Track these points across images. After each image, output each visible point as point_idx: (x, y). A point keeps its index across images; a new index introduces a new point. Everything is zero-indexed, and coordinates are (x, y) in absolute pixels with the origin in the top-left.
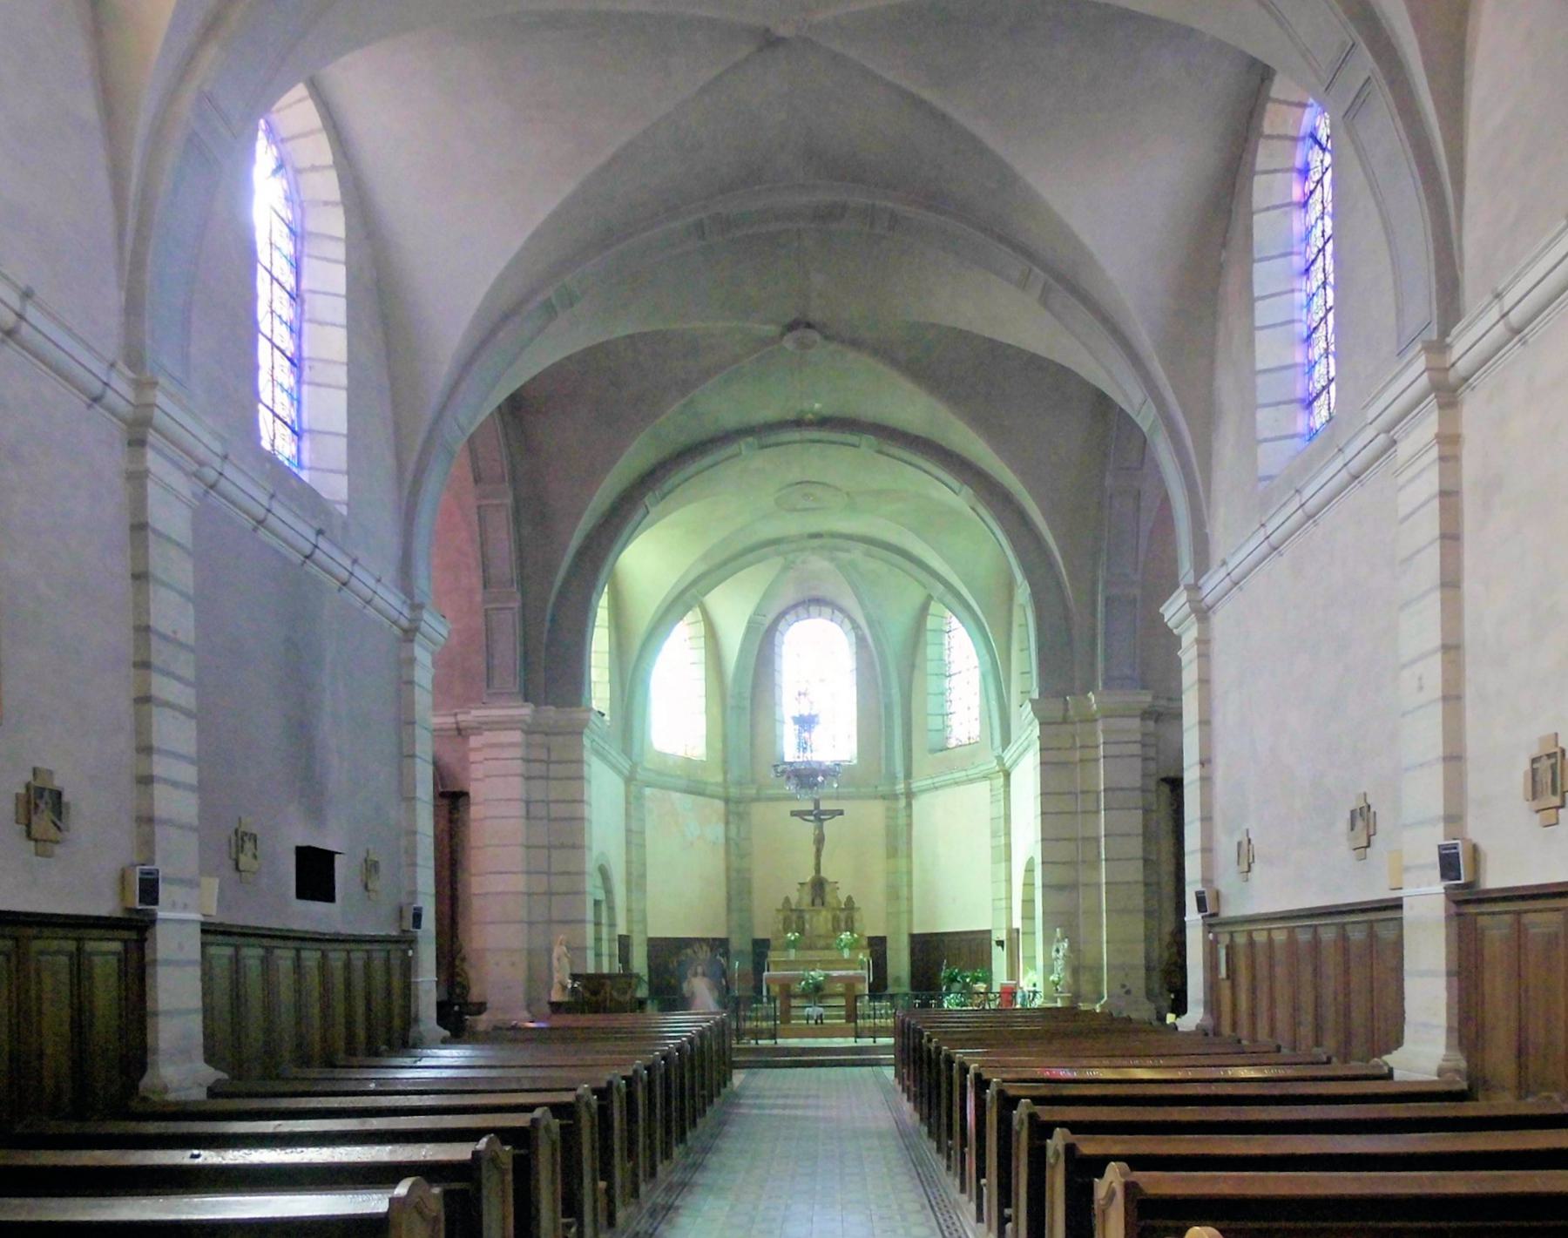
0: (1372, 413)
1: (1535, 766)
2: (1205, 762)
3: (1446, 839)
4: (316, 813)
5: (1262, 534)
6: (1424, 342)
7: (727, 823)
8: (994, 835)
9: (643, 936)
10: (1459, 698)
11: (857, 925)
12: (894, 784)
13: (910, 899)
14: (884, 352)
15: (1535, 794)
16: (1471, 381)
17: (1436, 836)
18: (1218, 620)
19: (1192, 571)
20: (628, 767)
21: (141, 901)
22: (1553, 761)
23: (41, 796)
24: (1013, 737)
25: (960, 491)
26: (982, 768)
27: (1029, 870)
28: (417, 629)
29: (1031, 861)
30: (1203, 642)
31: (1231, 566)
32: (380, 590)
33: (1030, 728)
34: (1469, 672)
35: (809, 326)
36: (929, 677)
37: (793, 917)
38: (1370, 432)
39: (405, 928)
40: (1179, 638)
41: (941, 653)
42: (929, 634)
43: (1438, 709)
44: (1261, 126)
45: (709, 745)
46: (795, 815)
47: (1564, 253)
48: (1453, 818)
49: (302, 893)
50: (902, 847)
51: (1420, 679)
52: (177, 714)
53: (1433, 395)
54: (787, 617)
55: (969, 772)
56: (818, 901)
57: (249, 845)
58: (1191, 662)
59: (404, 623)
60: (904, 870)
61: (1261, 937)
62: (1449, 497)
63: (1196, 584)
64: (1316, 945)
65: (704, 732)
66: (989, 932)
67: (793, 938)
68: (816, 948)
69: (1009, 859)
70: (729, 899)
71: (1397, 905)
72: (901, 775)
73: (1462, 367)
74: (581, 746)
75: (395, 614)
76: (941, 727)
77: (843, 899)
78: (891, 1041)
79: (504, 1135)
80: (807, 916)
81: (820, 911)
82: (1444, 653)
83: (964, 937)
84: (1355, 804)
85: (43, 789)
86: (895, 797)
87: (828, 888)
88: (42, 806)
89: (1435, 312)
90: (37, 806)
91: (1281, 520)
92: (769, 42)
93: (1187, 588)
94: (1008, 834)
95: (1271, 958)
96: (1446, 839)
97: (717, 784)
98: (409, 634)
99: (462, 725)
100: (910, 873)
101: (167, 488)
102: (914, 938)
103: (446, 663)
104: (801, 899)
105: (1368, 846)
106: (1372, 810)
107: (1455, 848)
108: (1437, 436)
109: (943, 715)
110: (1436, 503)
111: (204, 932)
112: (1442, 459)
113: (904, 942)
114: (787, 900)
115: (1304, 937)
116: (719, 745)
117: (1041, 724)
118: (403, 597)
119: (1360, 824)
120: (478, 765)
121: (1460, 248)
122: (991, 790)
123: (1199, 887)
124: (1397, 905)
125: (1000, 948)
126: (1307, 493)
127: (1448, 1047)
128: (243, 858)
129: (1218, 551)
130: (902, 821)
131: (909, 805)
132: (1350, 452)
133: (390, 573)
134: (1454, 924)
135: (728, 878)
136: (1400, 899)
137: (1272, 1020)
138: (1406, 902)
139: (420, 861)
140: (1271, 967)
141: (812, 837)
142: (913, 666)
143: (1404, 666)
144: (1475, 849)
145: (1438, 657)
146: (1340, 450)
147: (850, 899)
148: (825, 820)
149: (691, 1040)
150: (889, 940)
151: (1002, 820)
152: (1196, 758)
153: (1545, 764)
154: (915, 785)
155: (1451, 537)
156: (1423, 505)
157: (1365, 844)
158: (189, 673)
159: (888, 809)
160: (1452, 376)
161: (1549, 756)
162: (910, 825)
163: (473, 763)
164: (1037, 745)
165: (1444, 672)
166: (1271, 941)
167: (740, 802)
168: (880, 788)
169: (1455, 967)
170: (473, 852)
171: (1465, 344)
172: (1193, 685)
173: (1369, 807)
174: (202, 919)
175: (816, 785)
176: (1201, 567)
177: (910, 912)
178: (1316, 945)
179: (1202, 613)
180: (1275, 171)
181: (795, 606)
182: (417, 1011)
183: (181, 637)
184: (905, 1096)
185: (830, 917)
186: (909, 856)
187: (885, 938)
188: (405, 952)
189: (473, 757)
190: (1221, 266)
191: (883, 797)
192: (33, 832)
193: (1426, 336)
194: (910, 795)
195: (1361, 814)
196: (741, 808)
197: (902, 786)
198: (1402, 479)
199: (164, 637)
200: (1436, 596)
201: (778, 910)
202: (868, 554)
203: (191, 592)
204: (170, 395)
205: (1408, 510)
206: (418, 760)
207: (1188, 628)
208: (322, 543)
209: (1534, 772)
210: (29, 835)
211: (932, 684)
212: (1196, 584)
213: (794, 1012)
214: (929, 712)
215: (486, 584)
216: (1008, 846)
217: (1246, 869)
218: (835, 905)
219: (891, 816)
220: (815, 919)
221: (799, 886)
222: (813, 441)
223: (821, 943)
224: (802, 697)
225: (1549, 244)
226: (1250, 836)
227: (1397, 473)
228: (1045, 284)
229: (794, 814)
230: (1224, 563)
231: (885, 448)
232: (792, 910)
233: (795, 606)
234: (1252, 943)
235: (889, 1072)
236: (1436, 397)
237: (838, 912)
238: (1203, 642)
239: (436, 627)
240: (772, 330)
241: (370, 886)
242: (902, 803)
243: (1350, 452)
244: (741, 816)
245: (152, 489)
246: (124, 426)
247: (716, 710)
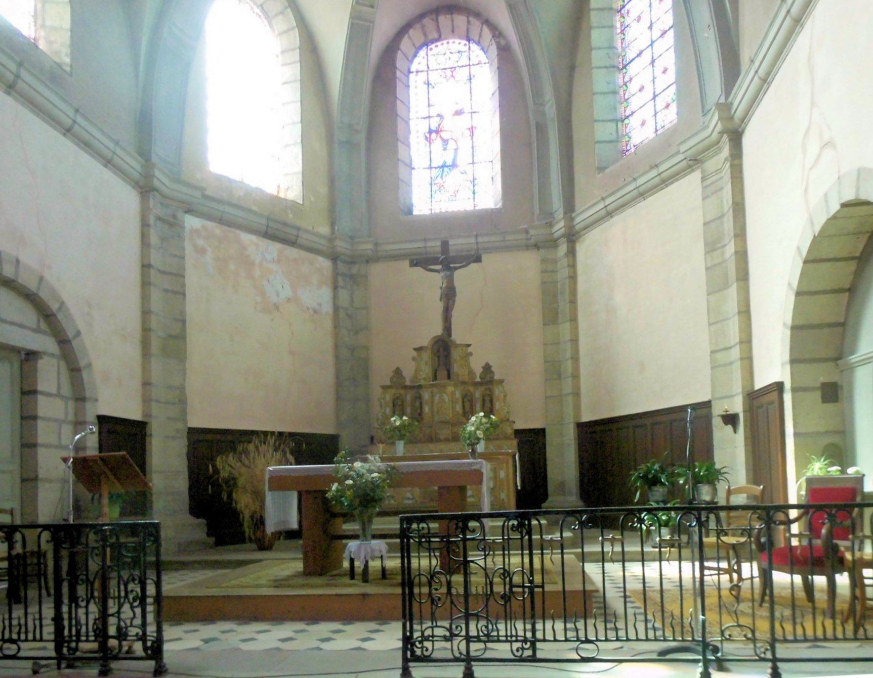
7: (335, 288)
8: (712, 246)
11: (497, 405)
12: (550, 225)
13: (576, 376)
20: (138, 167)
36: (595, 71)
41: (611, 40)
42: (593, 13)
45: (306, 184)
46: (416, 265)
50: (564, 307)
54: (411, 32)
56: (443, 373)
60: (568, 354)
65: (299, 168)
66: (707, 405)
67: (398, 423)
68: (438, 440)
70: (339, 384)
72: (560, 214)
76: (614, 137)
77: (478, 370)
80: (426, 396)
81: (444, 386)
86: (553, 243)
87: (456, 354)
94: (741, 234)
100: (575, 341)
102: (581, 426)
104: (417, 370)
109: (616, 121)
113: (570, 434)
114: (398, 372)
116: (323, 190)
125: (730, 427)
130: (563, 273)
131: (572, 252)
135: (337, 357)
141: (438, 293)
142: (572, 68)
147: (487, 368)
148: (456, 268)
150: (547, 431)
159: (544, 261)
162: (573, 278)
167: (353, 263)
177: (577, 394)
185: (458, 395)
186: (574, 319)
187: (541, 432)
191: (537, 246)
194: (572, 237)
196: (355, 269)
211: (600, 80)
214: (596, 117)
218: (466, 378)
219: (548, 269)
220: (437, 398)
221: (415, 353)
223: (445, 433)
224: (434, 135)
232: (405, 387)
237: (471, 389)
242: (563, 249)
244: (356, 280)
247: (320, 147)
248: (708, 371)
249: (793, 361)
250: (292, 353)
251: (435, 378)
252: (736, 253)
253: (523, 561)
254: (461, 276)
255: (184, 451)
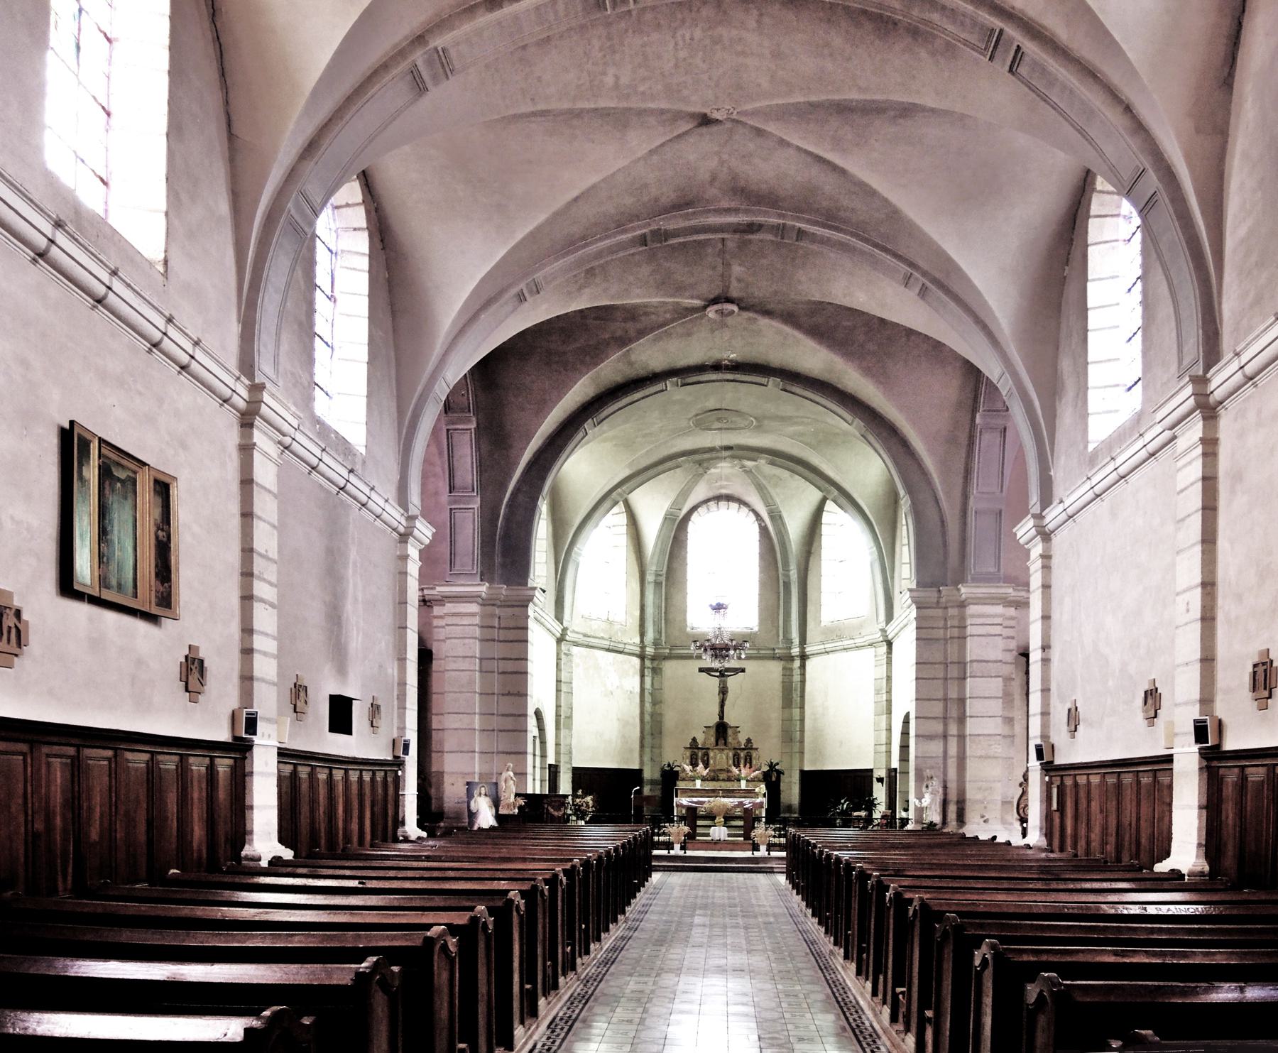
0: (1159, 415)
1: (1256, 669)
2: (1045, 647)
3: (1200, 716)
4: (341, 669)
5: (1087, 486)
6: (1190, 376)
8: (878, 692)
9: (569, 766)
10: (1213, 619)
13: (802, 741)
14: (790, 318)
15: (1254, 689)
16: (1225, 404)
17: (1195, 713)
18: (1056, 539)
19: (1038, 503)
21: (246, 733)
22: (1265, 667)
23: (193, 664)
24: (896, 615)
25: (853, 422)
26: (866, 638)
27: (906, 721)
28: (411, 534)
29: (907, 716)
30: (1046, 557)
31: (1067, 503)
32: (388, 508)
33: (909, 610)
34: (1220, 601)
35: (729, 300)
37: (697, 753)
38: (1158, 429)
39: (397, 754)
40: (1029, 551)
43: (1198, 625)
44: (1094, 184)
47: (1275, 336)
48: (1207, 700)
49: (333, 728)
51: (1188, 604)
52: (267, 606)
53: (1198, 411)
54: (699, 509)
55: (856, 641)
57: (302, 694)
58: (1036, 571)
59: (402, 529)
60: (798, 718)
61: (1082, 780)
62: (1209, 482)
63: (1041, 514)
64: (1119, 786)
68: (718, 780)
69: (889, 712)
71: (1169, 759)
72: (796, 641)
73: (1218, 395)
74: (527, 617)
75: (395, 524)
77: (743, 740)
78: (784, 854)
79: (390, 955)
80: (711, 754)
82: (1202, 588)
83: (859, 774)
84: (1147, 687)
85: (194, 659)
86: (791, 659)
87: (730, 732)
88: (194, 670)
89: (1201, 354)
90: (191, 670)
91: (1102, 476)
92: (705, 121)
93: (1034, 516)
94: (889, 692)
95: (1089, 793)
96: (1200, 716)
97: (634, 644)
98: (404, 537)
99: (427, 598)
100: (802, 720)
101: (265, 454)
103: (427, 555)
105: (1270, 697)
106: (1159, 691)
107: (1206, 722)
108: (1201, 439)
110: (1200, 484)
111: (280, 754)
112: (1205, 454)
113: (796, 777)
114: (694, 740)
115: (1111, 780)
117: (917, 608)
118: (402, 511)
119: (1150, 701)
120: (441, 630)
121: (1221, 314)
122: (875, 656)
123: (1039, 742)
124: (1169, 759)
126: (1119, 460)
127: (1197, 856)
128: (299, 704)
129: (1058, 491)
130: (797, 678)
131: (803, 667)
132: (1148, 437)
133: (391, 493)
134: (1205, 775)
136: (1172, 755)
137: (1088, 843)
138: (1175, 758)
139: (408, 705)
140: (1089, 802)
143: (1178, 594)
144: (1220, 722)
145: (1199, 590)
146: (1141, 435)
147: (749, 741)
149: (608, 853)
151: (885, 681)
152: (1039, 644)
153: (1261, 669)
154: (809, 650)
155: (1210, 508)
156: (1192, 484)
157: (1267, 696)
158: (274, 579)
159: (784, 669)
160: (1211, 399)
161: (1264, 664)
162: (803, 682)
163: (436, 627)
164: (914, 625)
165: (1203, 600)
166: (1089, 783)
168: (777, 651)
169: (1204, 802)
170: (434, 696)
171: (1222, 379)
172: (1038, 589)
173: (1157, 689)
174: (279, 745)
175: (727, 656)
176: (1046, 501)
178: (1119, 786)
179: (1046, 536)
180: (1106, 216)
181: (706, 501)
182: (404, 816)
183: (271, 555)
184: (795, 891)
186: (802, 707)
188: (397, 772)
189: (436, 622)
190: (1065, 278)
191: (780, 658)
192: (1021, 792)
193: (1193, 372)
194: (804, 657)
195: (1151, 694)
197: (798, 650)
198: (1180, 464)
199: (260, 554)
200: (1199, 548)
201: (686, 748)
202: (772, 463)
203: (276, 524)
204: (272, 395)
205: (1182, 486)
206: (408, 630)
207: (1035, 546)
208: (352, 479)
209: (1255, 673)
210: (187, 690)
212: (1041, 514)
213: (699, 831)
215: (452, 489)
216: (889, 702)
217: (1153, 716)
219: (788, 673)
222: (728, 381)
225: (1266, 329)
226: (1157, 685)
227: (1177, 459)
228: (923, 284)
229: (701, 670)
230: (1061, 502)
231: (789, 388)
233: (706, 501)
234: (1076, 785)
235: (782, 879)
236: (1200, 412)
238: (1046, 557)
239: (424, 531)
240: (697, 303)
241: (375, 724)
242: (797, 663)
243: (1148, 437)
245: (256, 454)
246: (239, 415)
248: (873, 753)
249: (900, 760)
250: (618, 719)
251: (717, 744)
252: (887, 700)
253: (945, 752)
254: (732, 682)
255: (570, 780)
